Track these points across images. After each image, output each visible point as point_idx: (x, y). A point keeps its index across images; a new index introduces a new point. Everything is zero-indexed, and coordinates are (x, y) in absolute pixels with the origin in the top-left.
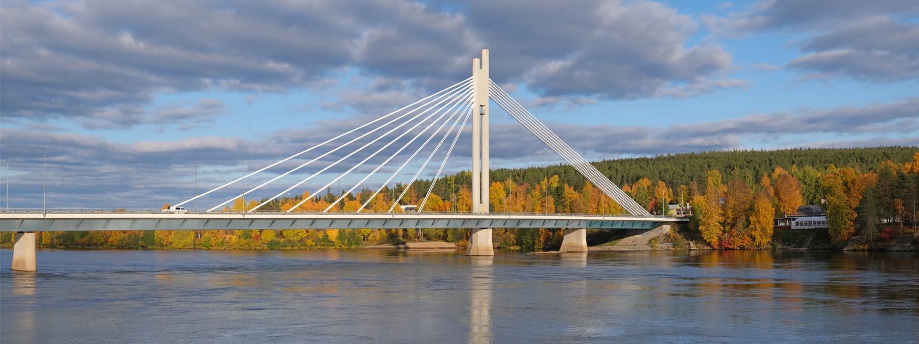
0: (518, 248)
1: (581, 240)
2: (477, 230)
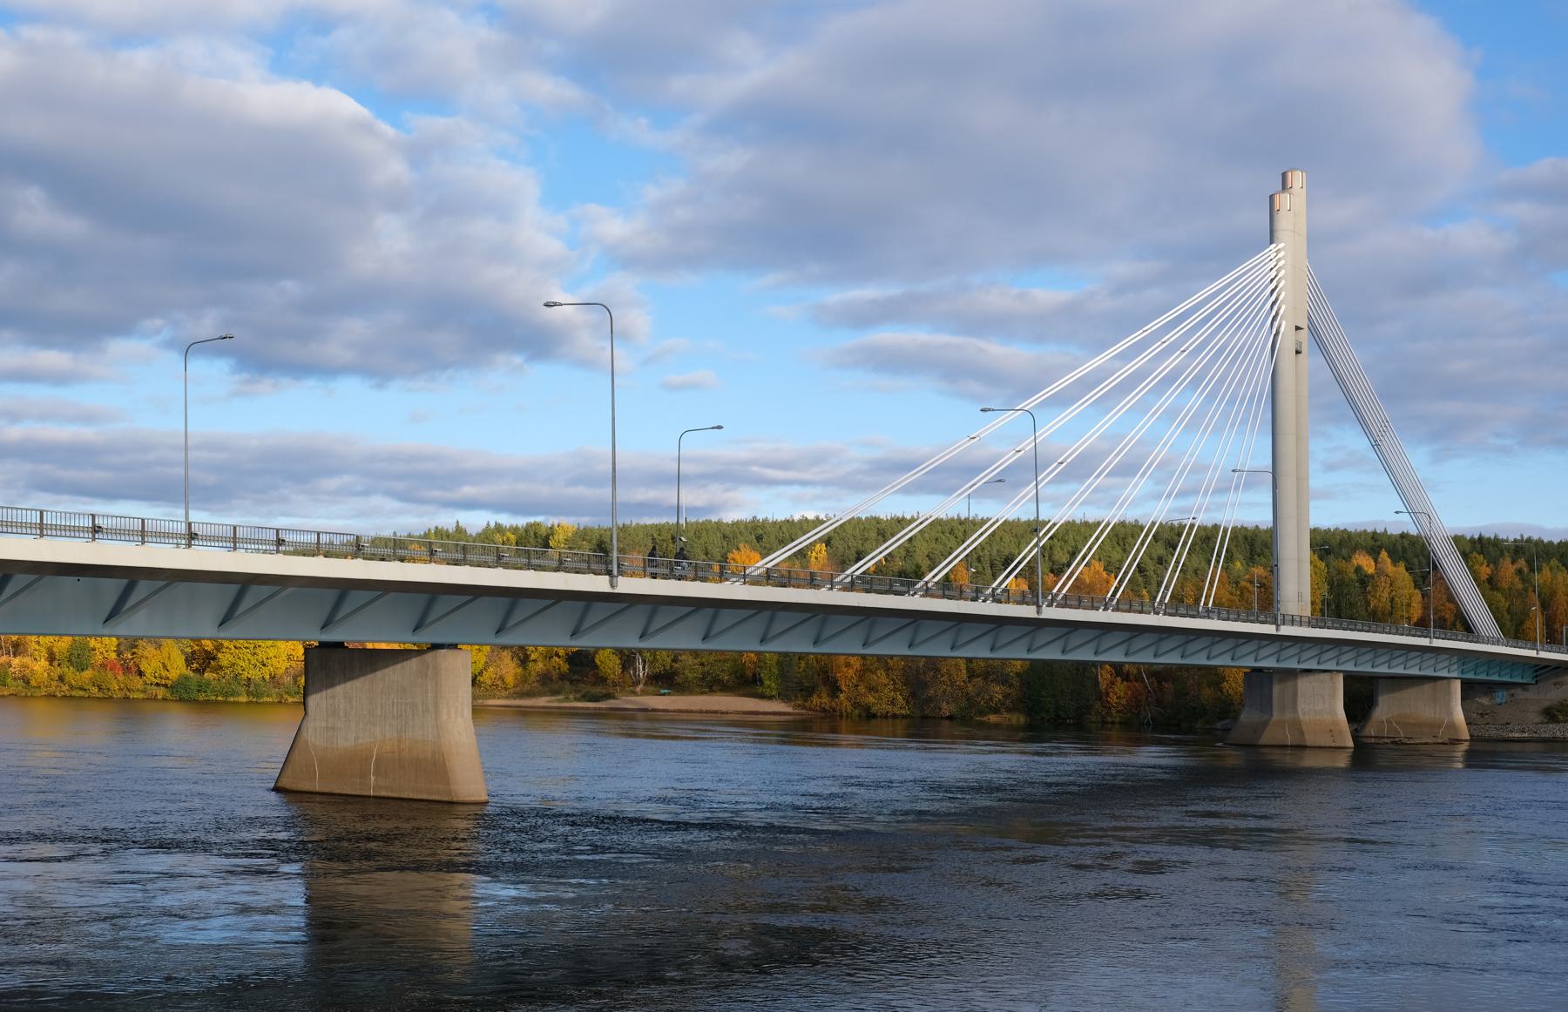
1: (1450, 713)
2: (1291, 674)
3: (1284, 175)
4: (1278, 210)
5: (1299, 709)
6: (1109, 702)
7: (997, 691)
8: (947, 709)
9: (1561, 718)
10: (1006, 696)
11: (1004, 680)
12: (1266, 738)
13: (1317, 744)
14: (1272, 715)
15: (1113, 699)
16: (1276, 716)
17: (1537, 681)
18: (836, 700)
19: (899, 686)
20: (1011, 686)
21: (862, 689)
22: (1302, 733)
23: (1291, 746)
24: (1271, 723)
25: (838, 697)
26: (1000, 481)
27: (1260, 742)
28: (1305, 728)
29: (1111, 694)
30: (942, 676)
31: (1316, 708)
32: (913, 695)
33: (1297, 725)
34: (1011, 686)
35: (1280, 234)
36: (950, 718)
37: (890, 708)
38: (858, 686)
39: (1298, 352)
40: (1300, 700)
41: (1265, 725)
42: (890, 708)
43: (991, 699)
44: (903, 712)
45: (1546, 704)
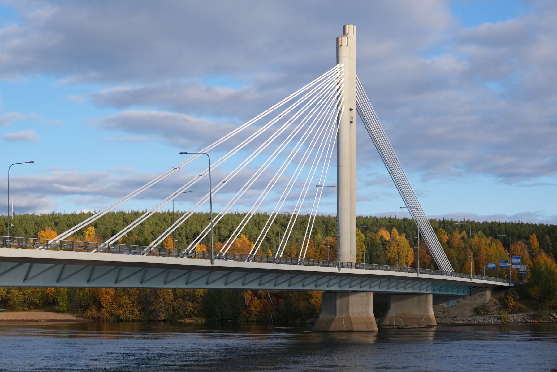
0: (202, 320)
1: (427, 311)
3: (344, 27)
4: (341, 46)
5: (350, 312)
6: (250, 310)
7: (190, 305)
8: (162, 316)
9: (482, 313)
10: (195, 308)
11: (194, 300)
12: (333, 327)
13: (359, 330)
14: (336, 315)
15: (252, 309)
16: (338, 316)
17: (470, 295)
18: (101, 312)
19: (136, 304)
20: (197, 303)
21: (115, 306)
22: (351, 324)
23: (346, 331)
24: (335, 319)
25: (101, 311)
26: (190, 192)
27: (330, 329)
28: (353, 321)
29: (251, 306)
30: (160, 298)
31: (359, 311)
32: (143, 309)
33: (349, 320)
34: (197, 303)
35: (342, 59)
36: (164, 321)
37: (130, 316)
38: (112, 304)
39: (351, 122)
40: (350, 307)
41: (332, 320)
42: (130, 316)
43: (186, 310)
44: (138, 318)
45: (475, 306)
